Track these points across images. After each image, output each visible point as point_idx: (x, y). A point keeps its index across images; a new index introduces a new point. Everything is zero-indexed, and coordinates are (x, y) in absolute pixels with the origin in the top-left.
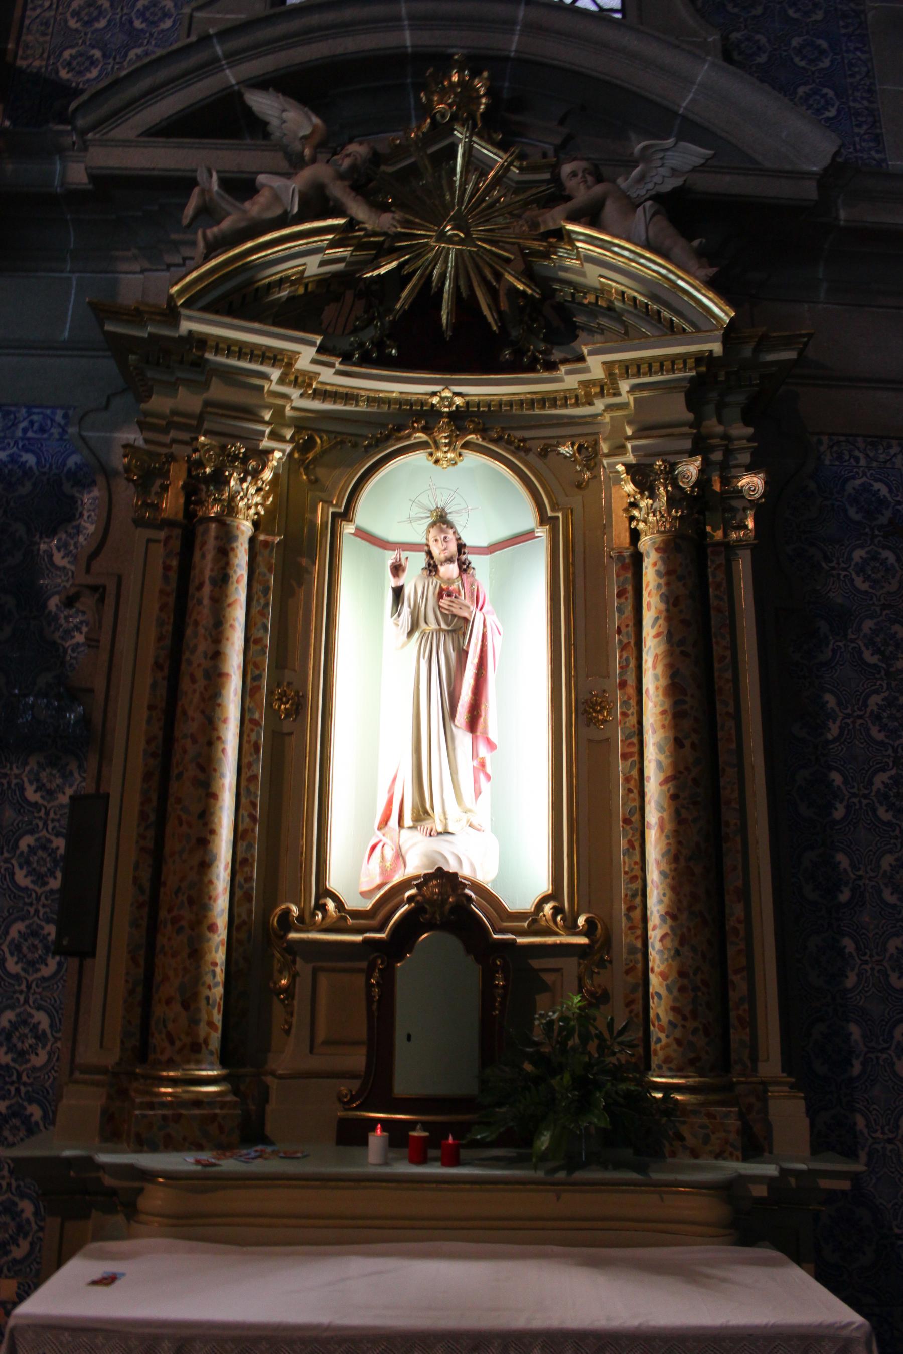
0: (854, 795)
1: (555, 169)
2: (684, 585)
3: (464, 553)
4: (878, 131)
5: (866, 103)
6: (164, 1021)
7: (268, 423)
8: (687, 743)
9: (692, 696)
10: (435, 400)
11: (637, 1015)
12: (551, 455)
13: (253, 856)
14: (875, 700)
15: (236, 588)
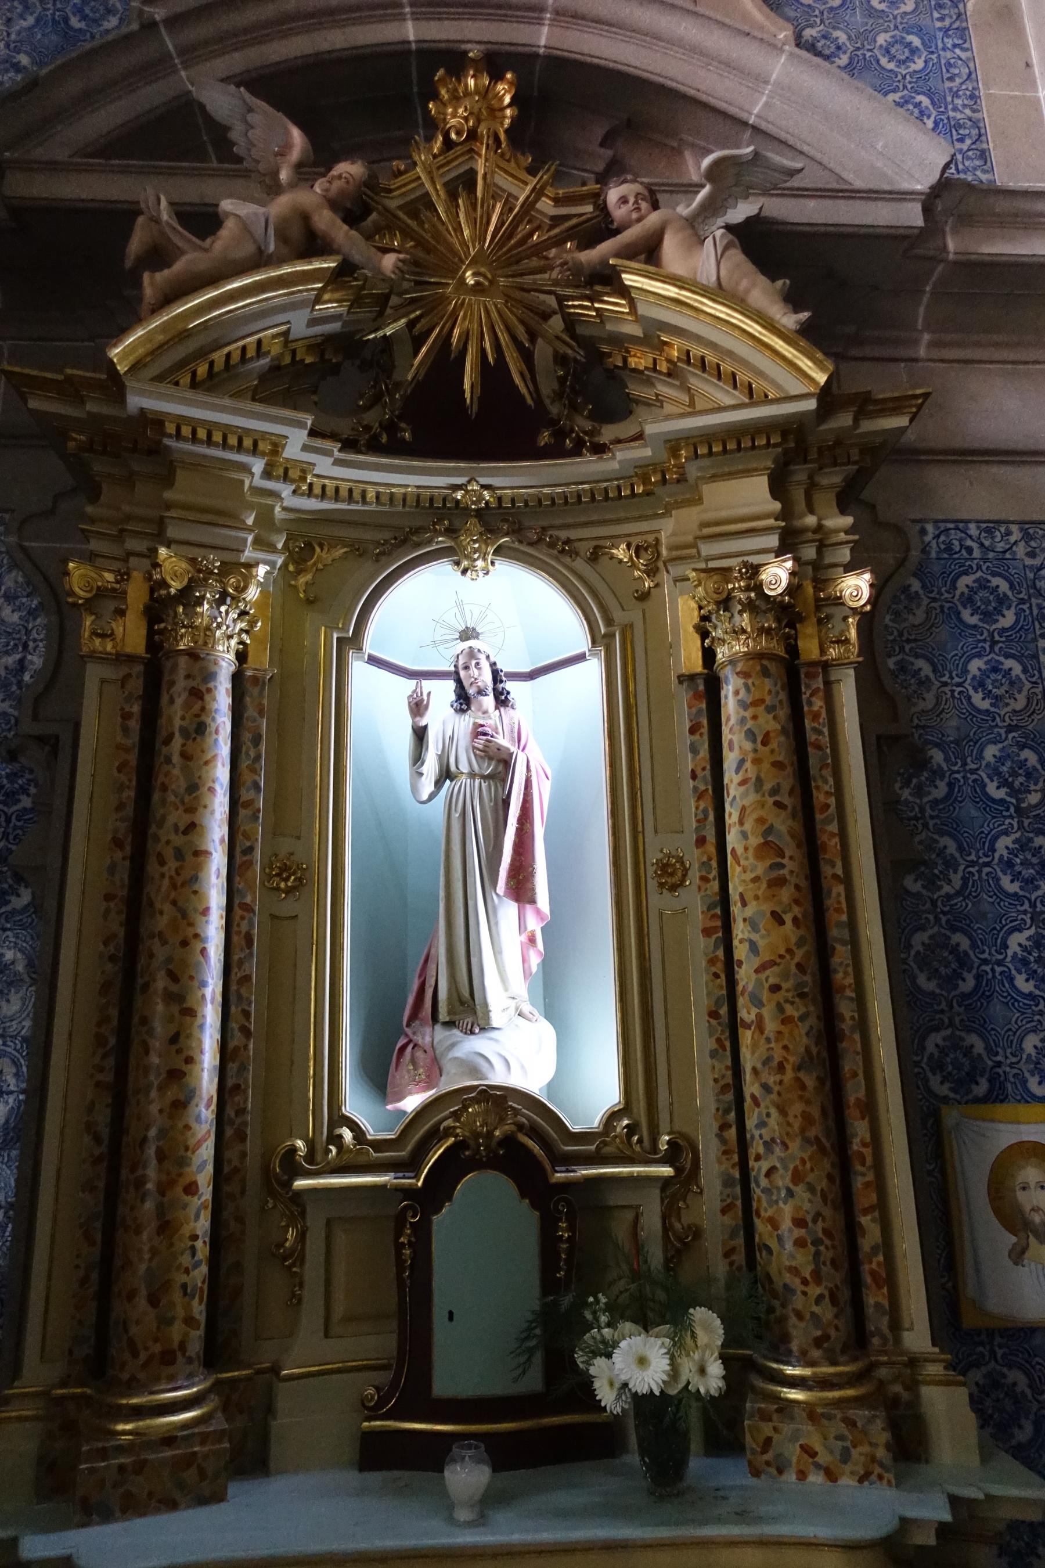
0: (985, 962)
1: (598, 199)
2: (775, 718)
3: (501, 681)
4: (985, 146)
5: (968, 112)
6: (125, 1322)
7: (250, 530)
8: (788, 918)
9: (791, 858)
10: (459, 495)
11: (739, 1268)
12: (604, 560)
13: (246, 1080)
14: (1004, 844)
15: (216, 740)
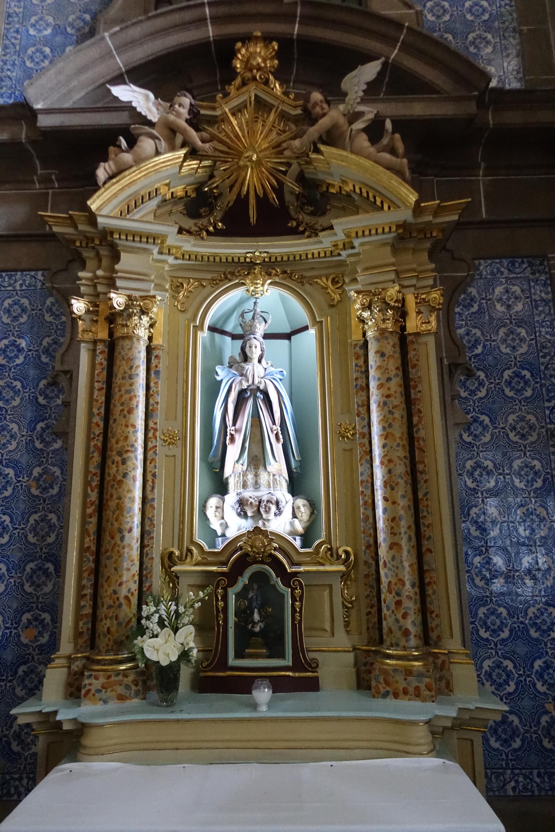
7: (152, 281)
